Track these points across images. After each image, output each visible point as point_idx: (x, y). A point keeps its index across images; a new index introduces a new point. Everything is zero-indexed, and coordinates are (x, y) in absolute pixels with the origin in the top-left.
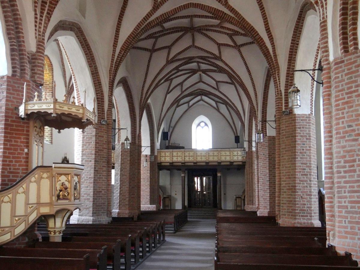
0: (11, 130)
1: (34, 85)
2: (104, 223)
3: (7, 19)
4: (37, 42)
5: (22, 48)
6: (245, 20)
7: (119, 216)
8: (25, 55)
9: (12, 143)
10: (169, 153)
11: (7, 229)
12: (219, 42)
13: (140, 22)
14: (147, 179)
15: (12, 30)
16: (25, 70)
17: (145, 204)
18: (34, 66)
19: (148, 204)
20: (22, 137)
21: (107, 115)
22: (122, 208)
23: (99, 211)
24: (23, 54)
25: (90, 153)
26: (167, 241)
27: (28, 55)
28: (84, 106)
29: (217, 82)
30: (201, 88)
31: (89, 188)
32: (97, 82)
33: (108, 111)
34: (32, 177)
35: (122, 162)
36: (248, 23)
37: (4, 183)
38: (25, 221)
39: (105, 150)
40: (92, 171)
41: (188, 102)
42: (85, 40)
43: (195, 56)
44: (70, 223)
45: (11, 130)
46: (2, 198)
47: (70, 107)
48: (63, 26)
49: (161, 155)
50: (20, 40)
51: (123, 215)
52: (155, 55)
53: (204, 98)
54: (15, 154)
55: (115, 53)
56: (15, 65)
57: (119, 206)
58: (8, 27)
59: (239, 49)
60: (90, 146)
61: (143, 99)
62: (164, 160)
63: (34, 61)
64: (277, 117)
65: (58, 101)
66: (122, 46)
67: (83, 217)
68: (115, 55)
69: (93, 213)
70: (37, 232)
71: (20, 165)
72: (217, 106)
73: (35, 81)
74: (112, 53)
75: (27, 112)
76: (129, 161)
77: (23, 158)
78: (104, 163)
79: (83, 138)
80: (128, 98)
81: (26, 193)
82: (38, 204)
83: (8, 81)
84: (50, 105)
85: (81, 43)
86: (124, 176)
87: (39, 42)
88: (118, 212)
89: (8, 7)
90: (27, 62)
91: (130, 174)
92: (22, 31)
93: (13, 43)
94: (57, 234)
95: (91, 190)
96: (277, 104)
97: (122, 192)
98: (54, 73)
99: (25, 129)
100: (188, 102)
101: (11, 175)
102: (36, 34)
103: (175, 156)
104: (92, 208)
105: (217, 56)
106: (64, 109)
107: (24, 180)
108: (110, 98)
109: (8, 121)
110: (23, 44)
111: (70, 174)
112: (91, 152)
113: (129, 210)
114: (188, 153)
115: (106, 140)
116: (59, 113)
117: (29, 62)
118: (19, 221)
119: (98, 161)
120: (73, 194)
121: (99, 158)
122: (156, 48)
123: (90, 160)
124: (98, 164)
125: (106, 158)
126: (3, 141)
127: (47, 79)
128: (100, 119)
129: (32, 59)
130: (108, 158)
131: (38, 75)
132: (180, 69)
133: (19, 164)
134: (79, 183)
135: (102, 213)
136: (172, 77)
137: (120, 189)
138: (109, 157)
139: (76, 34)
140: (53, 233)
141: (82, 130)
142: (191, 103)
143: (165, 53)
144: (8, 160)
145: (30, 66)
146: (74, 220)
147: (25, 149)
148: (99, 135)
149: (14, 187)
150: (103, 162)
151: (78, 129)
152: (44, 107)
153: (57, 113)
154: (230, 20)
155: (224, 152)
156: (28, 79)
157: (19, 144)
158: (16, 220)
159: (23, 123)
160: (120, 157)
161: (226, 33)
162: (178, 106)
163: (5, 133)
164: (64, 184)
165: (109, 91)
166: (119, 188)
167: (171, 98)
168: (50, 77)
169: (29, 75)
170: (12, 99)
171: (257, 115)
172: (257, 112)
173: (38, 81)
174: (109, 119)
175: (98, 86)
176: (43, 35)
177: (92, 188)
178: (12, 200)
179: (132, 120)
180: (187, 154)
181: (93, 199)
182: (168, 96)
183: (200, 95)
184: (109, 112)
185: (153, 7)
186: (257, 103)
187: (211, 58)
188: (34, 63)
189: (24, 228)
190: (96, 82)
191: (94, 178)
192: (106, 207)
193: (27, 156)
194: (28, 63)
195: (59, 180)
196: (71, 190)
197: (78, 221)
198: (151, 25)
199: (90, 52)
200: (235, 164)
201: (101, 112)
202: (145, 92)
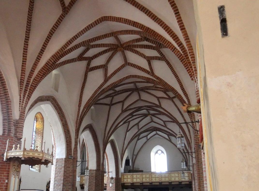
1: (15, 139)
3: (2, 102)
4: (20, 113)
5: (10, 118)
6: (167, 84)
12: (158, 96)
13: (96, 90)
15: (5, 108)
16: (11, 130)
18: (17, 128)
20: (5, 173)
21: (74, 152)
24: (10, 121)
25: (60, 179)
27: (14, 122)
28: (43, 152)
29: (164, 122)
32: (67, 130)
33: (74, 149)
35: (90, 184)
36: (170, 86)
39: (71, 177)
41: (147, 136)
42: (58, 105)
43: (143, 105)
47: (33, 153)
48: (41, 100)
49: (124, 178)
50: (9, 113)
52: (113, 107)
53: (158, 132)
56: (5, 129)
59: (173, 100)
61: (106, 137)
62: (126, 181)
63: (17, 124)
64: (196, 149)
65: (26, 150)
66: (85, 106)
68: (79, 112)
72: (169, 138)
73: (16, 137)
74: (77, 111)
75: (7, 157)
77: (4, 186)
78: (70, 186)
79: (56, 169)
80: (93, 138)
85: (55, 107)
87: (21, 113)
89: (3, 96)
90: (13, 126)
92: (11, 108)
96: (195, 140)
98: (44, 124)
100: (147, 136)
102: (20, 108)
103: (135, 178)
105: (158, 105)
106: (29, 155)
108: (76, 140)
110: (11, 115)
112: (61, 178)
115: (72, 170)
116: (26, 157)
117: (14, 125)
119: (65, 185)
121: (66, 183)
122: (113, 103)
123: (60, 184)
124: (65, 187)
125: (71, 182)
128: (68, 155)
129: (16, 123)
132: (134, 114)
138: (74, 181)
139: (51, 102)
141: (46, 166)
142: (149, 137)
143: (120, 105)
148: (67, 166)
154: (159, 83)
155: (174, 174)
156: (12, 136)
157: (2, 177)
159: (6, 164)
160: (88, 181)
161: (161, 91)
162: (138, 139)
165: (75, 135)
167: (130, 135)
169: (13, 134)
171: (191, 145)
172: (191, 144)
173: (19, 136)
179: (97, 153)
180: (144, 176)
182: (128, 133)
183: (155, 130)
184: (75, 150)
185: (104, 80)
186: (190, 137)
187: (154, 106)
188: (17, 125)
190: (66, 130)
193: (7, 185)
194: (13, 126)
198: (104, 91)
199: (61, 112)
200: (183, 183)
201: (69, 150)
202: (107, 133)
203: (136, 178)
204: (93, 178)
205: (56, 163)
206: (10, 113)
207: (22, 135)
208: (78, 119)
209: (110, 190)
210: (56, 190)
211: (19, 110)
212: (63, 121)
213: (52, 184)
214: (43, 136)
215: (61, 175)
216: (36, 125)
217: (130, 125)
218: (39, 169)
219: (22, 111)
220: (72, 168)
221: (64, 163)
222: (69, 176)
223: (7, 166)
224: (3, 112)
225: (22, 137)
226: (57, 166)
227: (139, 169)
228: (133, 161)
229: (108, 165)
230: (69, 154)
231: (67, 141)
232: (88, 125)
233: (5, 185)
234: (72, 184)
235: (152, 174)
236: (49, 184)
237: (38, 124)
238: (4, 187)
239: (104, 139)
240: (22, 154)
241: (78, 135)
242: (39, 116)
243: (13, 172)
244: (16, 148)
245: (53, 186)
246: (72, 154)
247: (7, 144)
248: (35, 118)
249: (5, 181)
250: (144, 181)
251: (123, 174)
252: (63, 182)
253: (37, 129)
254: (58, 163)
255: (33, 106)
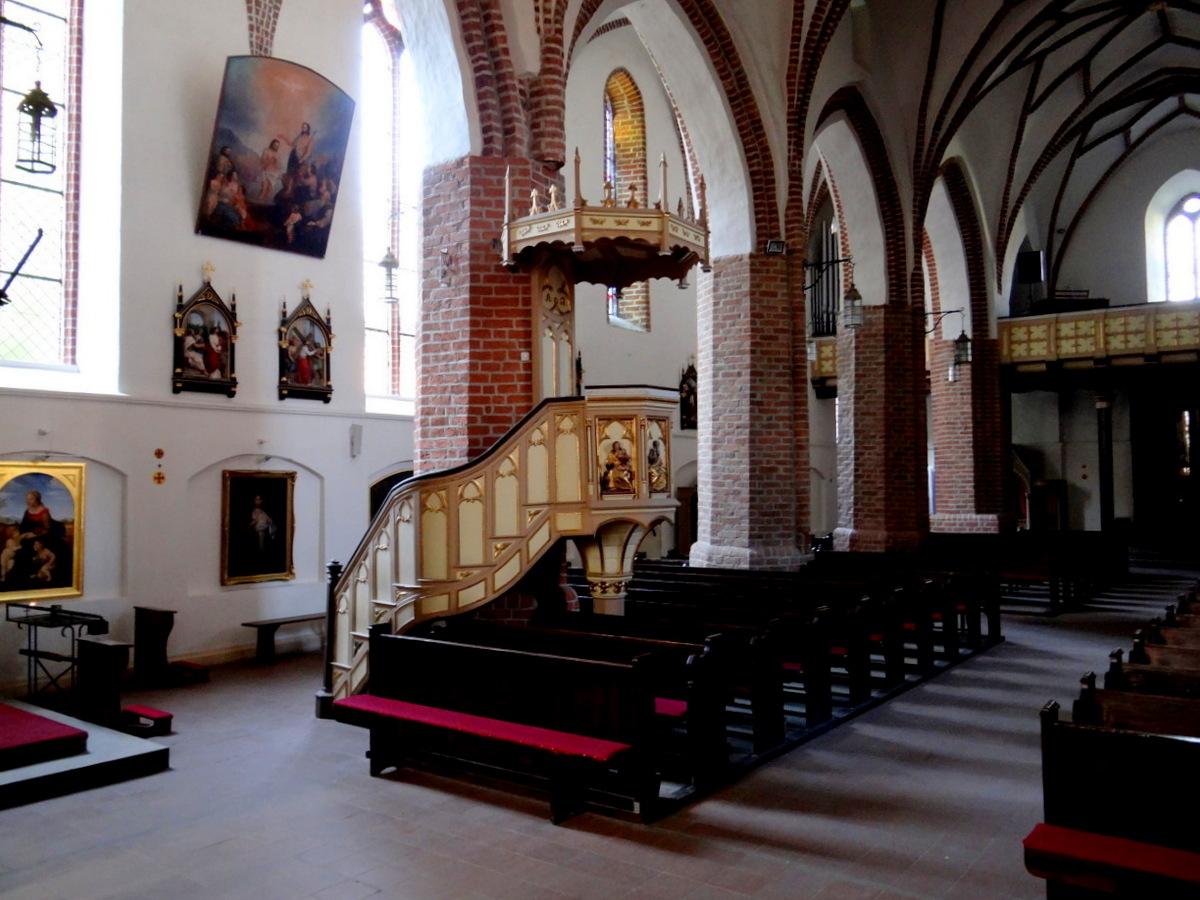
0: (488, 302)
2: (788, 570)
4: (541, 44)
5: (505, 70)
7: (854, 549)
8: (514, 87)
9: (489, 340)
10: (1044, 327)
11: (476, 572)
14: (962, 423)
15: (476, 26)
17: (958, 512)
18: (538, 115)
19: (968, 512)
20: (514, 320)
21: (787, 223)
22: (863, 522)
23: (770, 529)
25: (736, 349)
26: (1007, 639)
27: (522, 87)
28: (662, 208)
30: (1170, 65)
31: (736, 459)
32: (748, 121)
33: (788, 208)
34: (533, 431)
35: (861, 372)
37: (476, 448)
38: (519, 551)
39: (781, 336)
40: (746, 406)
41: (1124, 129)
44: (691, 565)
45: (488, 302)
46: (460, 489)
49: (1014, 338)
50: (496, 49)
51: (866, 548)
54: (498, 369)
55: (801, 15)
57: (855, 515)
58: (467, 21)
60: (737, 327)
61: (926, 147)
63: (535, 99)
65: (589, 204)
67: (725, 549)
69: (751, 537)
70: (566, 586)
71: (510, 400)
73: (540, 158)
76: (883, 367)
77: (521, 379)
78: (782, 379)
79: (716, 304)
81: (521, 473)
82: (553, 506)
83: (474, 171)
84: (549, 225)
85: (687, 11)
86: (867, 418)
87: (548, 40)
88: (853, 535)
90: (520, 107)
91: (885, 408)
92: (501, 23)
93: (481, 62)
94: (611, 593)
95: (742, 466)
97: (861, 469)
98: (647, 119)
99: (520, 296)
100: (1124, 129)
101: (491, 426)
102: (537, 20)
103: (1067, 338)
104: (748, 521)
107: (512, 438)
108: (794, 165)
109: (478, 281)
111: (635, 416)
112: (740, 346)
113: (887, 529)
114: (1122, 320)
116: (592, 240)
117: (524, 105)
118: (503, 552)
119: (761, 374)
120: (644, 474)
123: (736, 371)
126: (468, 335)
127: (628, 139)
128: (763, 239)
129: (533, 95)
130: (795, 360)
131: (548, 139)
133: (510, 394)
134: (665, 443)
135: (783, 536)
136: (1038, 49)
137: (856, 459)
138: (797, 356)
140: (598, 589)
141: (677, 281)
142: (1136, 131)
144: (482, 385)
145: (527, 117)
146: (698, 557)
147: (522, 354)
148: (763, 288)
149: (490, 458)
150: (780, 375)
151: (589, 284)
152: (554, 227)
153: (585, 240)
157: (507, 340)
158: (497, 549)
160: (853, 355)
162: (1080, 151)
163: (473, 312)
164: (617, 445)
165: (789, 143)
166: (852, 456)
167: (1041, 128)
168: (637, 130)
169: (525, 144)
170: (484, 218)
173: (549, 154)
174: (793, 236)
175: (751, 133)
176: (559, 17)
177: (747, 460)
178: (483, 493)
180: (1116, 325)
181: (751, 492)
182: (1031, 120)
184: (791, 212)
188: (537, 104)
189: (518, 571)
190: (744, 123)
191: (752, 425)
192: (792, 518)
195: (604, 436)
196: (639, 465)
197: (710, 559)
201: (767, 216)
203: (1072, 338)
204: (872, 343)
205: (712, 280)
206: (501, 46)
207: (562, 147)
208: (796, 61)
209: (947, 395)
210: (726, 394)
211: (535, 29)
212: (729, 75)
213: (706, 370)
214: (645, 178)
215: (740, 330)
216: (616, 130)
217: (1043, 73)
218: (642, 320)
219: (549, 31)
220: (785, 298)
221: (748, 275)
222: (773, 334)
223: (520, 291)
224: (471, 45)
225: (564, 158)
226: (721, 291)
227: (1088, 291)
228: (1055, 253)
229: (934, 284)
230: (766, 235)
231: (752, 174)
232: (841, 90)
233: (522, 372)
234: (789, 368)
235: (1157, 313)
236: (690, 375)
237: (623, 124)
238: (520, 381)
239: (918, 155)
240: (572, 225)
241: (802, 139)
242: (620, 87)
243: (547, 317)
244: (544, 201)
245: (712, 379)
246: (778, 234)
247: (504, 195)
248: (607, 98)
249: (519, 358)
250: (1115, 348)
251: (1010, 323)
252: (752, 359)
253: (618, 146)
254: (722, 279)
255: (595, 10)
